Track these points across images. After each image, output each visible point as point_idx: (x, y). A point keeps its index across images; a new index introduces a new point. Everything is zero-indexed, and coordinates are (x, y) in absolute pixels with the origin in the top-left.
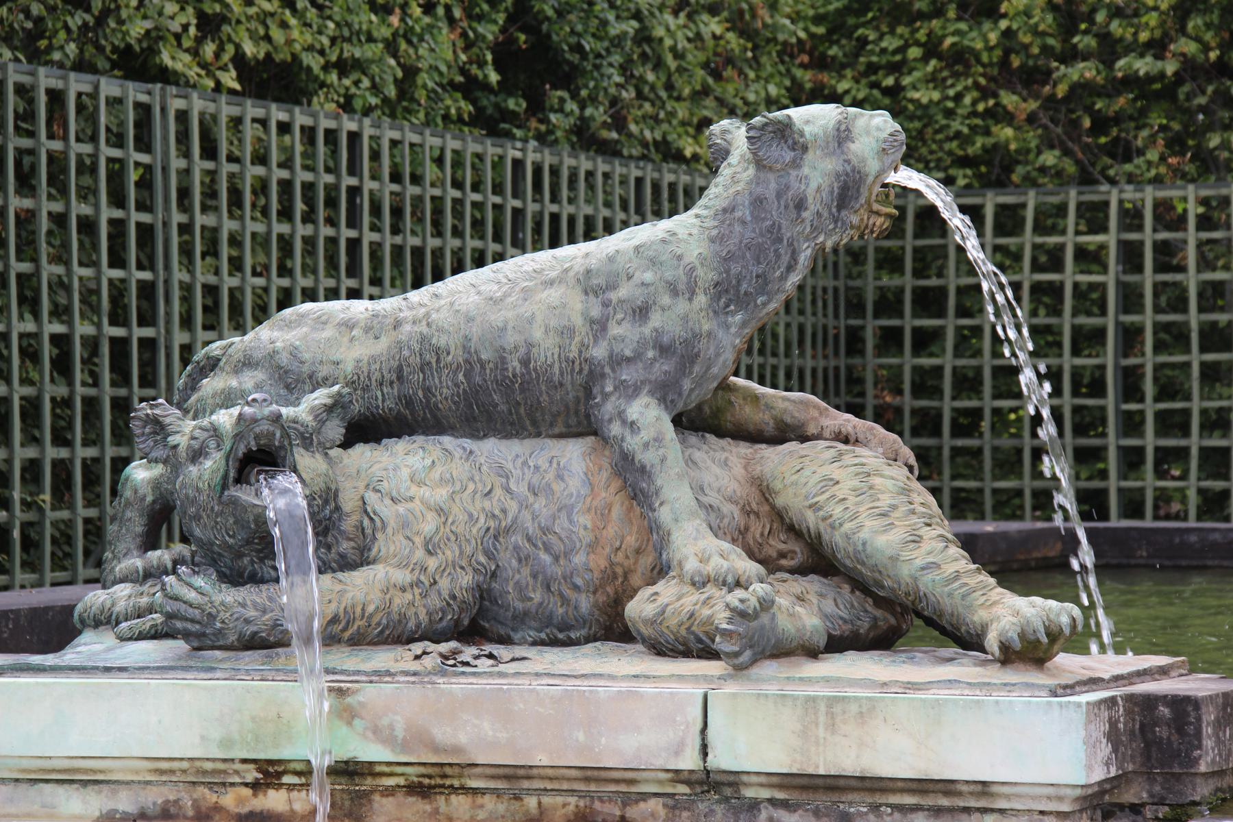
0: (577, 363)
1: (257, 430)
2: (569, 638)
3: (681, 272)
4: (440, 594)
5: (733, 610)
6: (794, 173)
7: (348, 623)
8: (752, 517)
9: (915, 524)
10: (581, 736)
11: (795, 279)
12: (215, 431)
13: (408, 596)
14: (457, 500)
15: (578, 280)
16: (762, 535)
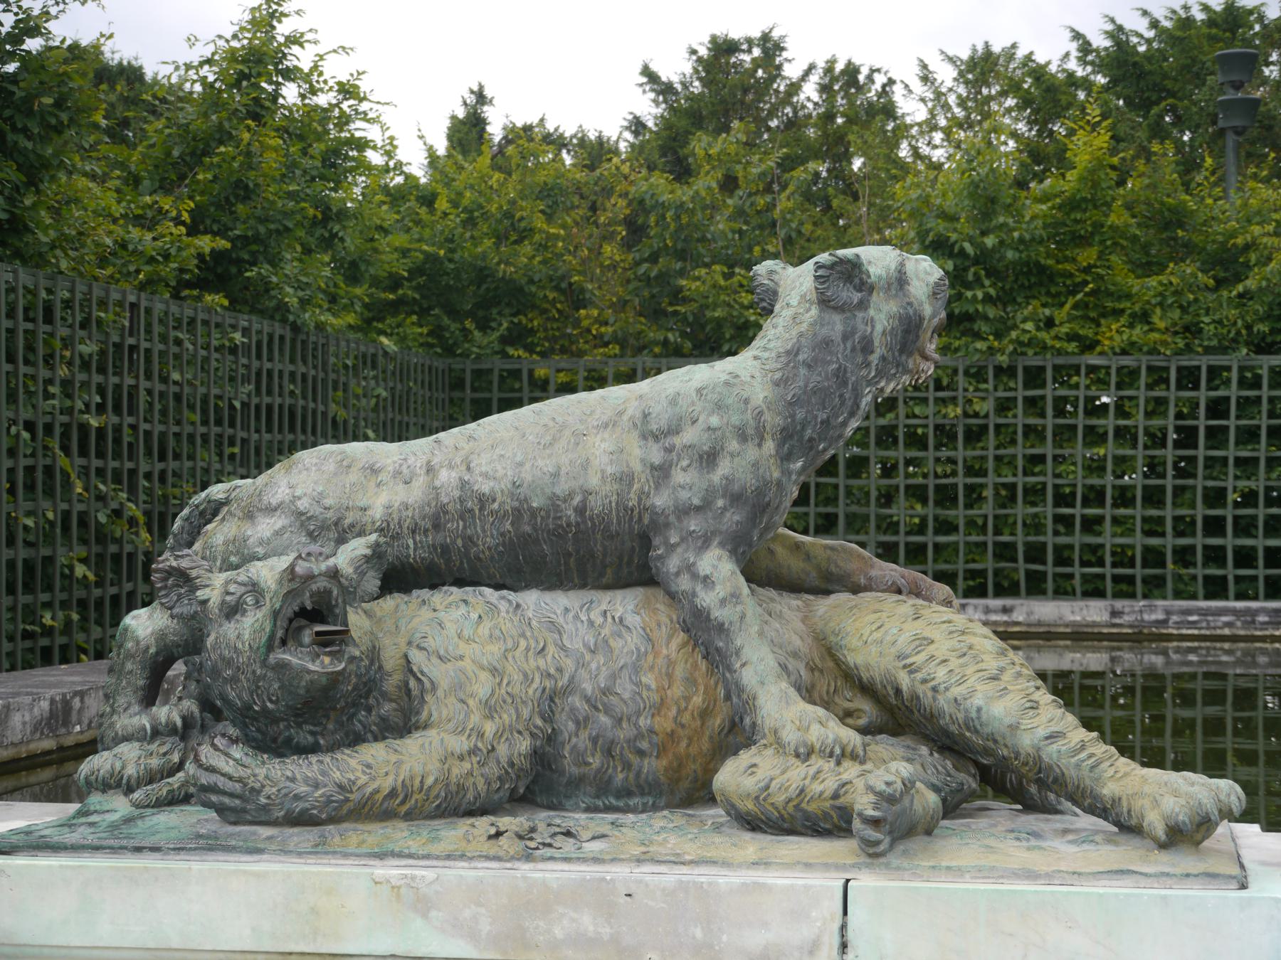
0: (636, 512)
1: (314, 587)
2: (628, 805)
3: (749, 417)
4: (498, 762)
5: (879, 794)
6: (860, 315)
7: (406, 796)
8: (817, 674)
9: (1027, 688)
10: (699, 933)
11: (854, 424)
12: (254, 588)
13: (467, 765)
14: (510, 659)
15: (635, 425)
16: (828, 692)
